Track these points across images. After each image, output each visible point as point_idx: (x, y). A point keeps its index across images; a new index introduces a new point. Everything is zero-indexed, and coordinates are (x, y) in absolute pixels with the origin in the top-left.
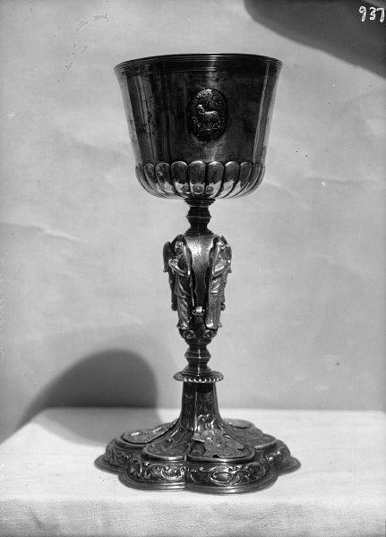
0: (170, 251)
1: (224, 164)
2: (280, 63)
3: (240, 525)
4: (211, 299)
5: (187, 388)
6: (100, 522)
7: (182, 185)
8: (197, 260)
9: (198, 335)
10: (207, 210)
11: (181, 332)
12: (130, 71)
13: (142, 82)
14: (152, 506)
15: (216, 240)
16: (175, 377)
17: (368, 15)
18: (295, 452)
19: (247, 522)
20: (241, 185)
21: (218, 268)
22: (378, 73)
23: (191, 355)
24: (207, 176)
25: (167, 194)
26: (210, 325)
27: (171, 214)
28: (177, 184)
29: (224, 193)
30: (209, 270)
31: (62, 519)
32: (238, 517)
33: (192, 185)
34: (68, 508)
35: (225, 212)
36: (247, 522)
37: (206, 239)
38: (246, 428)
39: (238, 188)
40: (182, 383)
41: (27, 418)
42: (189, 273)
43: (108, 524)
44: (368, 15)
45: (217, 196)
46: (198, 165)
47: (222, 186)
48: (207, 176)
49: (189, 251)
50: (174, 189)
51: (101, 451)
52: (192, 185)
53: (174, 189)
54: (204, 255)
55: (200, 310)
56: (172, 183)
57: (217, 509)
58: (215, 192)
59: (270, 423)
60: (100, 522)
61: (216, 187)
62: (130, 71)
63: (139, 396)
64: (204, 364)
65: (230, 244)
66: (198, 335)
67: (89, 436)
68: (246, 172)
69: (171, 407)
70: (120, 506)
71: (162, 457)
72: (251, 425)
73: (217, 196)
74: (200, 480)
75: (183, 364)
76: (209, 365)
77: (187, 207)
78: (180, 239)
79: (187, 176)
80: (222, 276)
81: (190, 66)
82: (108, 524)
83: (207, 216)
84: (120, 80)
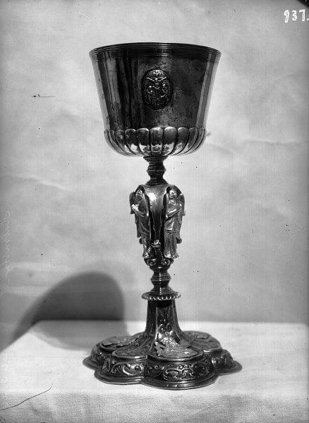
0: (134, 199)
1: (177, 128)
2: (220, 53)
3: (195, 412)
4: (166, 235)
5: (152, 306)
6: (82, 411)
7: (144, 147)
8: (154, 203)
9: (159, 260)
10: (151, 176)
11: (146, 260)
12: (100, 55)
13: (111, 65)
14: (125, 398)
15: (168, 190)
16: (143, 297)
17: (291, 16)
18: (236, 356)
19: (198, 411)
20: (189, 146)
21: (171, 211)
22: (54, 291)
23: (155, 281)
24: (165, 139)
25: (133, 153)
26: (169, 256)
27: (135, 168)
28: (140, 146)
29: (176, 151)
30: (164, 211)
31: (53, 407)
32: (190, 407)
33: (152, 146)
34: (56, 346)
35: (176, 166)
36: (198, 411)
37: (161, 185)
38: (207, 339)
39: (186, 149)
40: (147, 301)
41: (18, 334)
42: (148, 214)
43: (89, 412)
44: (291, 16)
45: (171, 153)
46: (157, 131)
47: (175, 146)
48: (165, 139)
49: (147, 198)
50: (139, 149)
51: (84, 354)
52: (152, 146)
53: (139, 149)
54: (159, 201)
55: (157, 243)
56: (137, 145)
57: (174, 400)
58: (170, 150)
59: (226, 336)
60: (82, 411)
61: (171, 146)
62: (100, 55)
63: (112, 313)
64: (165, 284)
65: (183, 193)
66: (159, 260)
67: (76, 346)
68: (191, 137)
69: (135, 319)
70: (98, 398)
71: (130, 357)
72: (208, 336)
73: (171, 153)
74: (158, 374)
75: (150, 287)
76: (171, 285)
77: (147, 164)
78: (141, 188)
79: (150, 140)
80: (178, 216)
81: (148, 52)
82: (89, 412)
83: (162, 169)
84: (94, 63)
